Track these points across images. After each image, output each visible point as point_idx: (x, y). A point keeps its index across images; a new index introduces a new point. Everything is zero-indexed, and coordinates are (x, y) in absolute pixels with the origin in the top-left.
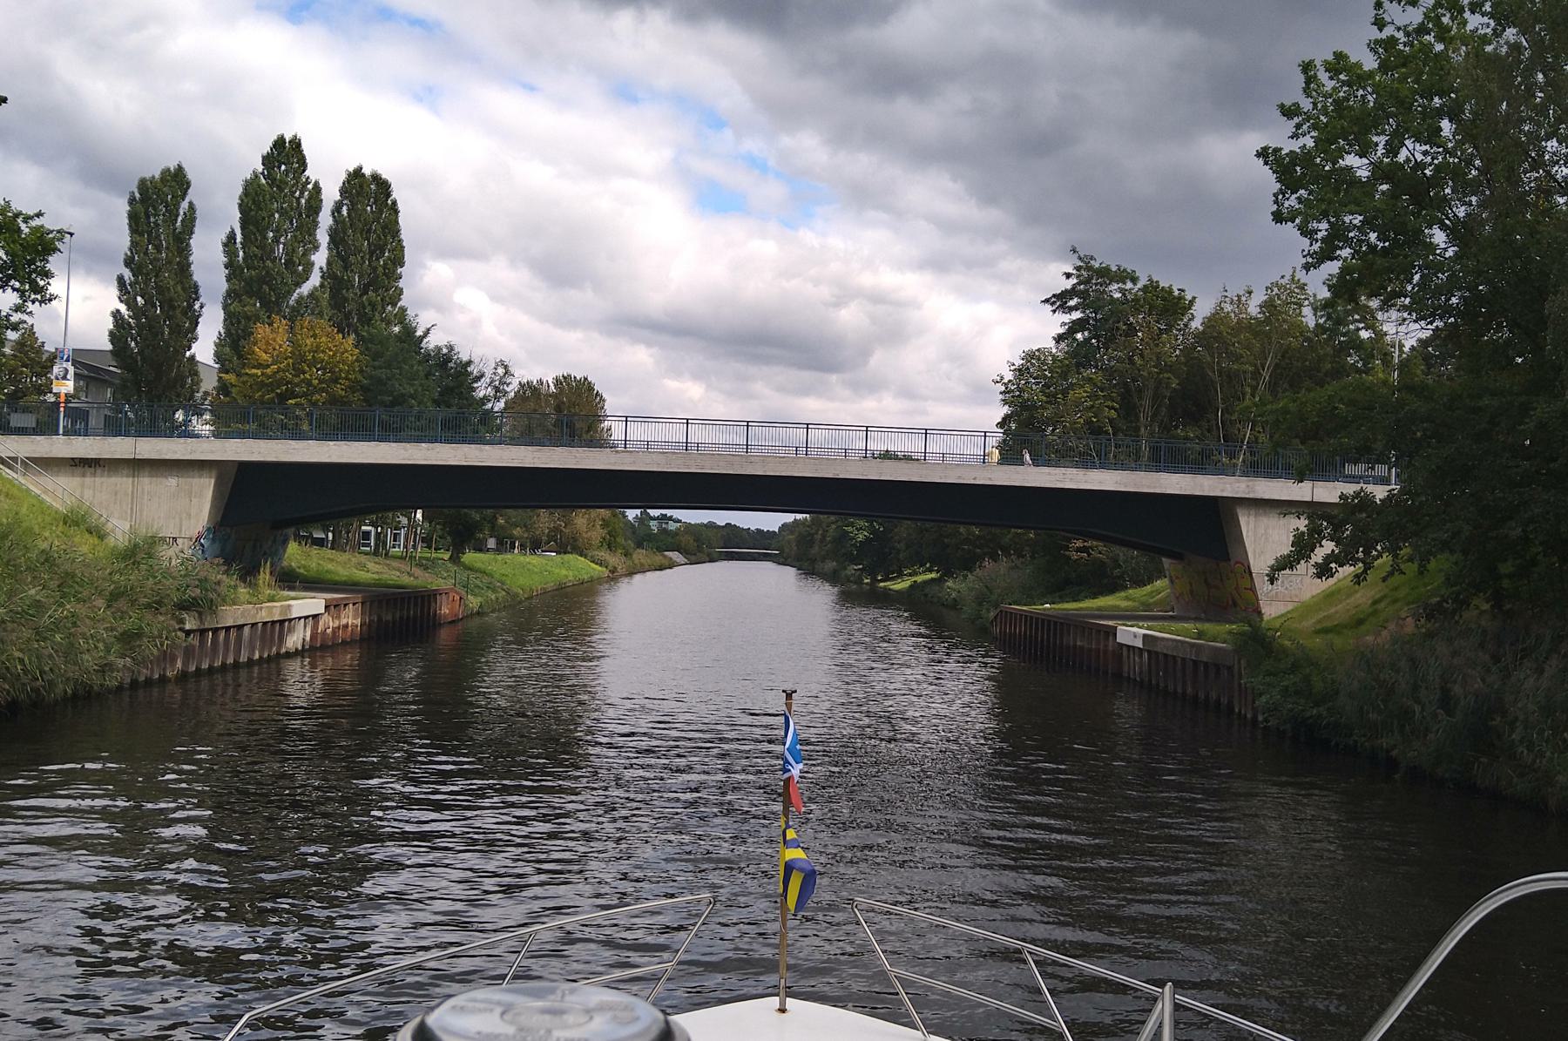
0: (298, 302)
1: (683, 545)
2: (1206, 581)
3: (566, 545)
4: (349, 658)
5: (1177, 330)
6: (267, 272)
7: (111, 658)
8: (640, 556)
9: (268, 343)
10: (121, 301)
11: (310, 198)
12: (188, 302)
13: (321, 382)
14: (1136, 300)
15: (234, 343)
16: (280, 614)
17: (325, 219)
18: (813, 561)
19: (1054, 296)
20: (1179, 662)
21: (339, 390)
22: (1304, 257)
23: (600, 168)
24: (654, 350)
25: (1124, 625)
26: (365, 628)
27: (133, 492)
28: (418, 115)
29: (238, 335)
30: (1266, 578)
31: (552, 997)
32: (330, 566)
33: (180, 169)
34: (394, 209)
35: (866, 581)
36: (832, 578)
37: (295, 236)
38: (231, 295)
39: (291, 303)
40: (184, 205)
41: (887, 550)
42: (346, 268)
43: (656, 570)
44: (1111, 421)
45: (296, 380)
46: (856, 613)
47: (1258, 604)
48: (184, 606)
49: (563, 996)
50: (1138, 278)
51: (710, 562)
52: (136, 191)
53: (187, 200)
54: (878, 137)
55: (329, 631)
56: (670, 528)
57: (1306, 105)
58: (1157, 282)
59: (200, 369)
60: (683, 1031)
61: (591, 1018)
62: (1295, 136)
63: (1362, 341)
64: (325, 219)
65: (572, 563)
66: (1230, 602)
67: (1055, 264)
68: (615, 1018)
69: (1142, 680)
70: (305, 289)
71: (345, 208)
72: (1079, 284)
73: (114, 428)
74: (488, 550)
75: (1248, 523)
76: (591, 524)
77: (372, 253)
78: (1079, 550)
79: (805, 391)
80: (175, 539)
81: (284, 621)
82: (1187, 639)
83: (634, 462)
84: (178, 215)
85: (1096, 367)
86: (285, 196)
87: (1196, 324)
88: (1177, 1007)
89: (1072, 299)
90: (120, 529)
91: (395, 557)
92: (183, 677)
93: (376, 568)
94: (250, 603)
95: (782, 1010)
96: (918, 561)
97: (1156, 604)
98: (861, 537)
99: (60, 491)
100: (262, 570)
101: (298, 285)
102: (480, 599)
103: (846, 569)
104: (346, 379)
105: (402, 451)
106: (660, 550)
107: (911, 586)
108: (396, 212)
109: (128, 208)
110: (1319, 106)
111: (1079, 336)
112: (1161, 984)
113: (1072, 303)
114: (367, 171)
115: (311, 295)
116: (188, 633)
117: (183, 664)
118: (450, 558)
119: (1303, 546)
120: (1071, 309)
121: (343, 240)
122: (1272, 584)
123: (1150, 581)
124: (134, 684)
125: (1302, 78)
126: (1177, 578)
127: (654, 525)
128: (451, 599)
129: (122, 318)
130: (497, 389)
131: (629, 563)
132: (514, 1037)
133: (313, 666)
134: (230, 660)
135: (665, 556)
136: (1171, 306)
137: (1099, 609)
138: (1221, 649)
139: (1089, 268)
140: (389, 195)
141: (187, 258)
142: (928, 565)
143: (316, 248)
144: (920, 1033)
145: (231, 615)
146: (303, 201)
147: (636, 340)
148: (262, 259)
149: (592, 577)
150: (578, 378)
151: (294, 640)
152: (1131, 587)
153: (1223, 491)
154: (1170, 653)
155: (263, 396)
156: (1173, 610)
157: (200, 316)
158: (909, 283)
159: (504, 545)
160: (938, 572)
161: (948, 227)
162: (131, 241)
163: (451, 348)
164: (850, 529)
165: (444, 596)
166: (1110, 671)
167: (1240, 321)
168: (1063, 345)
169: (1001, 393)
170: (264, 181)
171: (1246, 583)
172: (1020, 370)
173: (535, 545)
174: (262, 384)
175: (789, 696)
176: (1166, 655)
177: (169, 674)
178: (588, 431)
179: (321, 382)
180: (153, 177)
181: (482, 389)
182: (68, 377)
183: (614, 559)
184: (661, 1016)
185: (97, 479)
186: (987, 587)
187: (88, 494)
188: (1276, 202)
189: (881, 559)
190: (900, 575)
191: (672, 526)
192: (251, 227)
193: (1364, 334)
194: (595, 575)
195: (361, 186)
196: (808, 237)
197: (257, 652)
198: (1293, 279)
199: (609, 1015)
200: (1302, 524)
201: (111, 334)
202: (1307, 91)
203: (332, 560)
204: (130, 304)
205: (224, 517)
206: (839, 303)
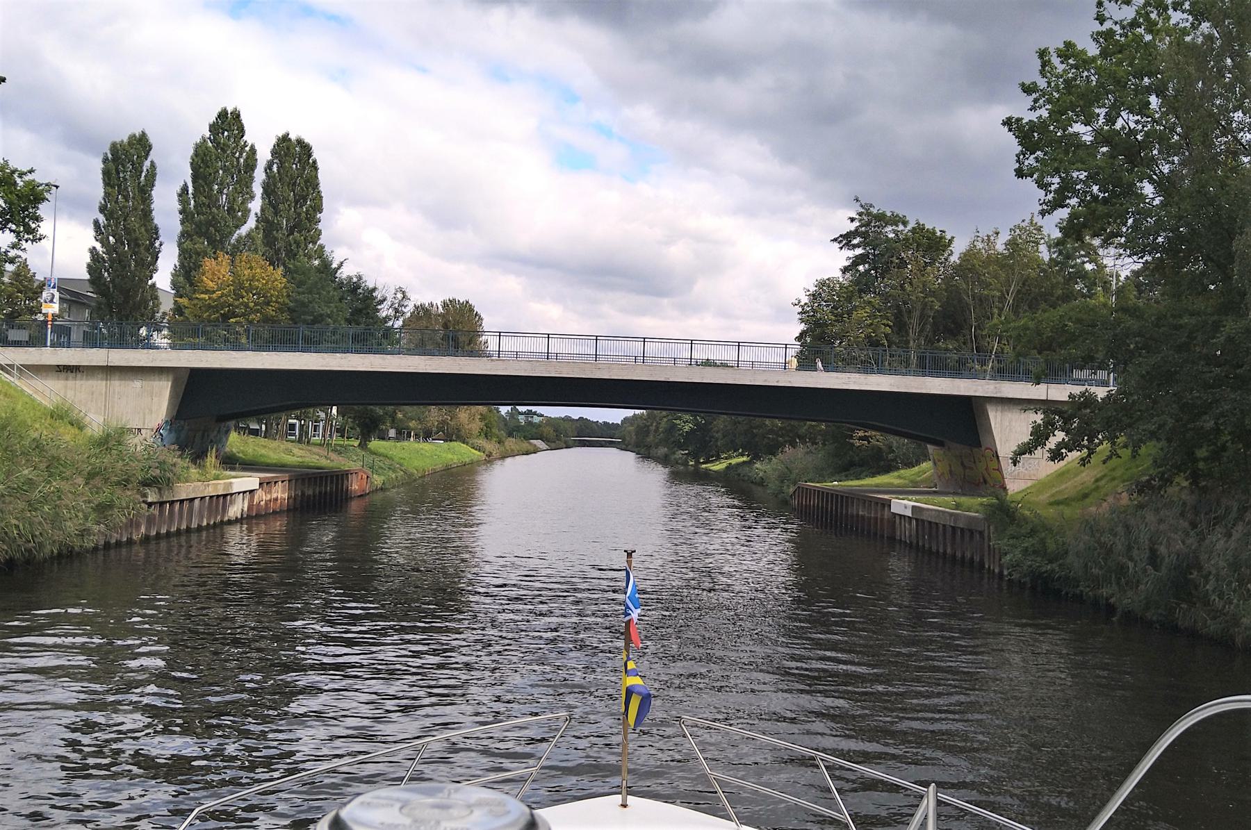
0: (238, 241)
2: (962, 464)
3: (451, 434)
4: (278, 525)
5: (939, 263)
6: (213, 217)
8: (511, 443)
10: (97, 240)
12: (150, 241)
13: (256, 304)
14: (906, 239)
16: (224, 490)
17: (259, 175)
18: (649, 447)
19: (841, 236)
21: (270, 311)
22: (1040, 205)
25: (896, 498)
26: (291, 501)
27: (106, 393)
29: (190, 268)
30: (1010, 461)
31: (441, 795)
32: (263, 451)
33: (144, 134)
34: (314, 166)
35: (691, 463)
36: (664, 461)
37: (236, 189)
38: (184, 235)
39: (232, 241)
40: (147, 164)
45: (236, 303)
46: (683, 488)
47: (1004, 481)
48: (147, 483)
52: (109, 152)
55: (262, 503)
57: (1042, 83)
59: (160, 294)
61: (472, 812)
62: (1033, 108)
63: (1087, 272)
64: (259, 175)
65: (456, 449)
66: (982, 480)
68: (491, 811)
69: (911, 543)
70: (244, 230)
71: (275, 166)
72: (861, 226)
73: (91, 341)
76: (472, 418)
78: (861, 438)
79: (642, 312)
80: (139, 430)
81: (227, 495)
82: (947, 510)
83: (506, 369)
84: (142, 172)
85: (875, 293)
86: (228, 156)
87: (954, 259)
88: (939, 803)
90: (96, 423)
92: (146, 539)
93: (300, 453)
94: (200, 481)
95: (624, 806)
96: (733, 447)
97: (922, 481)
98: (687, 428)
99: (48, 392)
100: (209, 454)
101: (238, 227)
102: (383, 478)
103: (674, 453)
104: (276, 302)
105: (321, 360)
106: (527, 438)
108: (316, 169)
109: (103, 166)
110: (1053, 84)
111: (861, 268)
112: (926, 784)
113: (855, 242)
114: (293, 137)
115: (248, 235)
116: (150, 505)
117: (146, 529)
119: (1039, 436)
120: (855, 246)
121: (273, 191)
122: (1015, 465)
123: (918, 463)
124: (107, 546)
125: (1039, 62)
126: (939, 461)
127: (522, 418)
128: (360, 477)
129: (97, 254)
130: (397, 311)
131: (502, 449)
133: (250, 531)
134: (184, 527)
135: (531, 444)
136: (934, 244)
137: (877, 486)
138: (974, 518)
139: (869, 214)
140: (310, 156)
141: (149, 206)
142: (740, 451)
143: (252, 198)
144: (734, 823)
145: (184, 491)
146: (242, 160)
148: (209, 206)
149: (472, 460)
150: (461, 302)
151: (235, 510)
153: (975, 391)
156: (936, 486)
158: (726, 226)
159: (403, 434)
162: (105, 193)
163: (360, 278)
164: (678, 422)
166: (878, 533)
167: (989, 256)
168: (848, 275)
170: (210, 144)
171: (993, 465)
172: (814, 295)
173: (427, 435)
174: (210, 307)
175: (630, 555)
176: (930, 523)
177: (135, 537)
178: (469, 344)
179: (256, 304)
180: (122, 141)
181: (385, 310)
182: (55, 300)
183: (490, 446)
184: (527, 810)
185: (77, 382)
186: (787, 468)
187: (70, 394)
188: (1018, 161)
189: (703, 445)
190: (718, 458)
191: (536, 419)
193: (1089, 267)
194: (475, 458)
195: (288, 149)
197: (205, 520)
198: (1031, 223)
199: (486, 809)
200: (1039, 418)
201: (89, 266)
202: (1043, 73)
203: (265, 447)
204: (104, 243)
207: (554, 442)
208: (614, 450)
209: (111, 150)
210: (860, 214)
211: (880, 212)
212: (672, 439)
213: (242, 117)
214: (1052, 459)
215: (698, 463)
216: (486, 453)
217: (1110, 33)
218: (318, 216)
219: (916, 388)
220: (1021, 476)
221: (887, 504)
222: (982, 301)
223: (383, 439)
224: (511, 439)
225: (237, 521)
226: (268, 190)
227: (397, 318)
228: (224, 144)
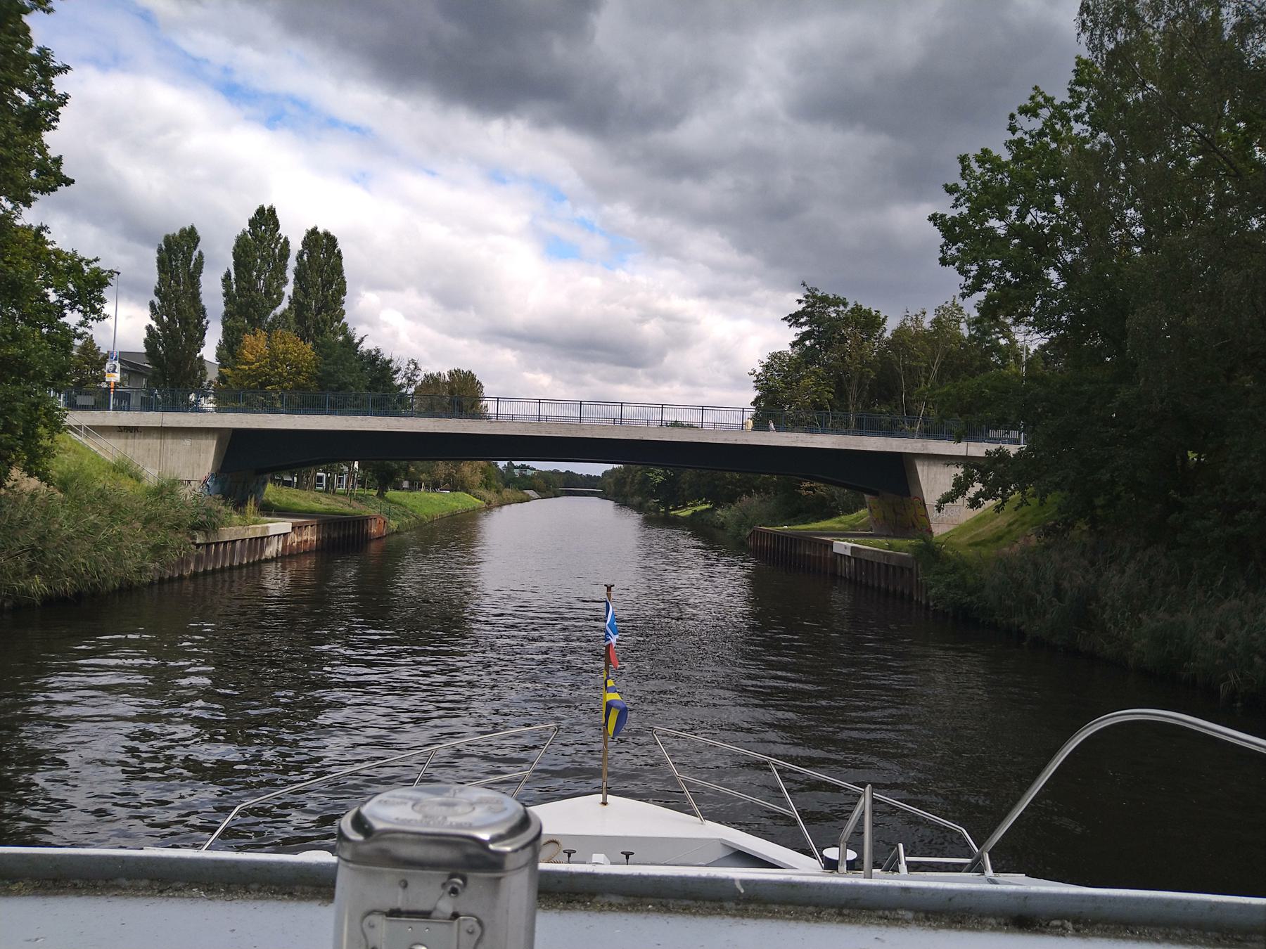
0: (273, 319)
2: (894, 510)
4: (308, 563)
6: (253, 299)
7: (146, 563)
8: (507, 493)
9: (252, 348)
13: (289, 374)
14: (846, 318)
15: (229, 348)
17: (292, 263)
19: (790, 315)
21: (301, 380)
23: (479, 228)
24: (517, 352)
26: (319, 542)
28: (355, 192)
31: (447, 794)
32: (295, 500)
36: (638, 508)
40: (196, 253)
41: (676, 489)
42: (307, 295)
46: (655, 532)
49: (454, 794)
51: (555, 497)
52: (162, 243)
53: (198, 250)
54: (670, 207)
55: (295, 544)
57: (963, 185)
59: (207, 365)
60: (537, 818)
61: (474, 809)
62: (955, 206)
63: (1001, 346)
64: (292, 263)
68: (490, 808)
69: (850, 578)
70: (278, 310)
71: (305, 255)
72: (807, 307)
73: (147, 406)
74: (403, 489)
75: (923, 471)
76: (474, 471)
77: (324, 287)
78: (807, 489)
80: (189, 481)
81: (264, 537)
84: (191, 260)
85: (819, 364)
86: (265, 247)
87: (887, 335)
88: (874, 801)
90: (152, 475)
91: (339, 494)
92: (195, 575)
93: (328, 501)
95: (605, 803)
96: (698, 496)
97: (862, 525)
98: (658, 480)
101: (274, 308)
103: (647, 502)
106: (521, 489)
107: (692, 514)
108: (341, 258)
110: (972, 185)
112: (863, 785)
113: (802, 320)
114: (321, 230)
115: (283, 315)
116: (198, 546)
119: (960, 487)
121: (304, 277)
123: (856, 510)
125: (960, 166)
129: (153, 330)
130: (409, 379)
132: (421, 821)
133: (284, 568)
134: (227, 564)
135: (525, 493)
136: (869, 322)
138: (904, 556)
139: (814, 296)
140: (335, 246)
143: (286, 283)
145: (227, 534)
146: (277, 251)
147: (505, 346)
151: (271, 550)
152: (843, 514)
153: (906, 448)
154: (869, 559)
156: (871, 530)
157: (206, 329)
158: (691, 307)
159: (415, 485)
161: (718, 268)
163: (378, 351)
164: (650, 475)
167: (917, 333)
168: (796, 349)
170: (250, 237)
172: (767, 366)
174: (249, 376)
175: (609, 589)
177: (185, 574)
178: (472, 408)
179: (289, 374)
181: (399, 380)
183: (489, 495)
184: (521, 807)
189: (672, 494)
190: (685, 506)
191: (529, 473)
193: (1003, 342)
194: (477, 506)
196: (621, 274)
199: (486, 806)
200: (960, 471)
202: (963, 176)
203: (297, 496)
206: (643, 320)
208: (595, 499)
209: (165, 242)
210: (807, 297)
213: (278, 213)
215: (668, 510)
216: (487, 501)
217: (1021, 141)
219: (855, 446)
221: (830, 544)
223: (398, 489)
226: (299, 275)
227: (410, 386)
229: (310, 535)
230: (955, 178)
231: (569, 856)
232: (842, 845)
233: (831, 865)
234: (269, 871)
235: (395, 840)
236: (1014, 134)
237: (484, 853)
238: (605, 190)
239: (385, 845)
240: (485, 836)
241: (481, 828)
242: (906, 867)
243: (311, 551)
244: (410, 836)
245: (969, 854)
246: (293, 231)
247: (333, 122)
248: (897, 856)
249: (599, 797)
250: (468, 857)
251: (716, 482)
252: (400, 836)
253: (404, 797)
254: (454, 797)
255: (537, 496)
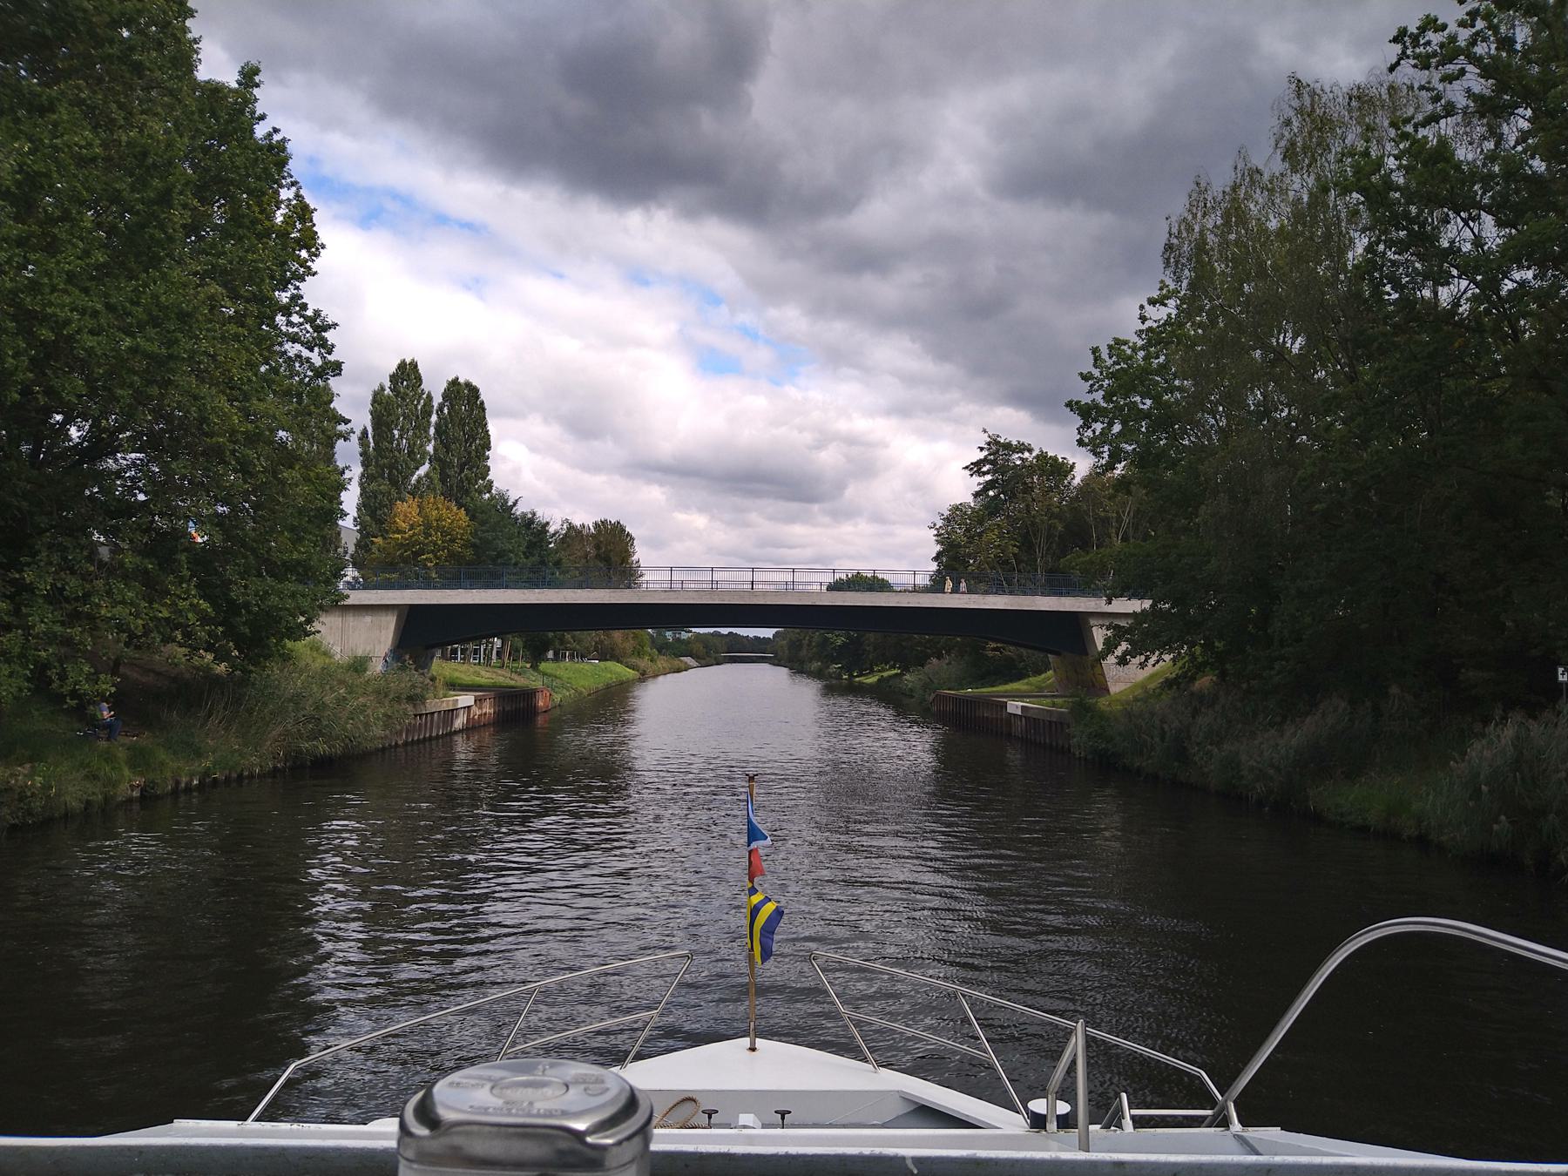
1: (694, 651)
2: (1076, 671)
3: (606, 654)
6: (396, 460)
8: (662, 662)
9: (406, 516)
11: (424, 405)
18: (802, 662)
19: (972, 464)
20: (1042, 724)
21: (456, 547)
23: (617, 341)
28: (467, 300)
29: (376, 508)
32: (456, 674)
34: (482, 408)
35: (844, 677)
36: (817, 675)
39: (413, 482)
43: (674, 672)
44: (1015, 555)
49: (544, 1070)
50: (1032, 449)
51: (717, 664)
54: (847, 308)
55: (476, 717)
56: (683, 638)
57: (1096, 373)
58: (1046, 453)
62: (1090, 392)
67: (1001, 408)
72: (990, 455)
74: (548, 660)
79: (792, 519)
83: (677, 598)
87: (1077, 481)
88: (1090, 1042)
89: (984, 466)
92: (406, 744)
93: (488, 675)
95: (753, 1049)
97: (1047, 687)
98: (839, 642)
103: (828, 667)
104: (461, 539)
108: (484, 410)
111: (991, 493)
113: (985, 469)
114: (461, 380)
118: (531, 667)
120: (984, 474)
121: (445, 432)
133: (468, 739)
134: (427, 735)
135: (681, 661)
138: (1062, 712)
140: (478, 397)
146: (419, 408)
147: (649, 482)
150: (613, 522)
151: (459, 723)
155: (402, 554)
160: (899, 668)
161: (910, 380)
165: (540, 693)
169: (935, 536)
178: (622, 564)
188: (1079, 433)
189: (855, 659)
190: (872, 671)
192: (384, 428)
195: (458, 392)
196: (792, 391)
202: (1095, 366)
205: (400, 642)
206: (820, 445)
207: (704, 659)
208: (766, 666)
210: (989, 444)
211: (1007, 441)
212: (828, 654)
214: (1119, 664)
218: (487, 453)
220: (1122, 679)
222: (1105, 521)
224: (662, 657)
225: (461, 731)
228: (404, 393)
229: (488, 709)
230: (1088, 366)
231: (710, 1117)
232: (1050, 1096)
233: (1038, 1122)
234: (323, 1159)
235: (468, 1134)
236: (1143, 323)
237: (578, 1146)
238: (769, 291)
239: (458, 1140)
240: (580, 1126)
241: (577, 1115)
242: (1131, 1123)
243: (489, 724)
244: (487, 1129)
245: (1209, 1102)
246: (434, 386)
247: (441, 220)
248: (1120, 1109)
249: (746, 1041)
250: (561, 1153)
251: (904, 644)
252: (475, 1128)
253: (480, 1078)
254: (544, 1074)
255: (695, 664)
